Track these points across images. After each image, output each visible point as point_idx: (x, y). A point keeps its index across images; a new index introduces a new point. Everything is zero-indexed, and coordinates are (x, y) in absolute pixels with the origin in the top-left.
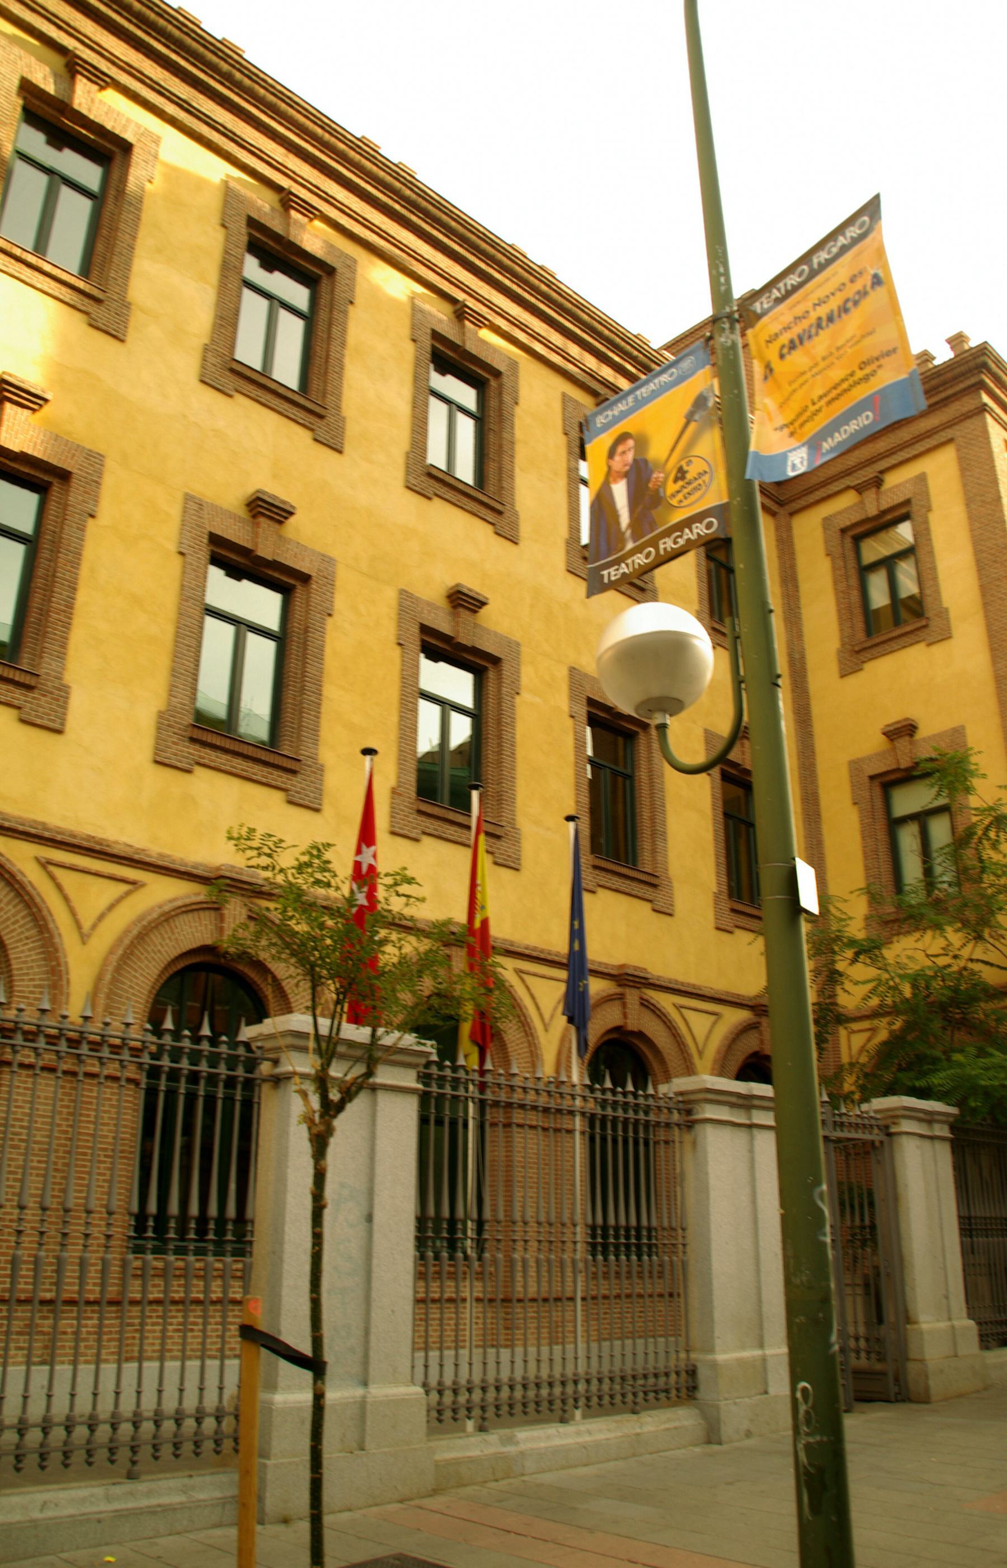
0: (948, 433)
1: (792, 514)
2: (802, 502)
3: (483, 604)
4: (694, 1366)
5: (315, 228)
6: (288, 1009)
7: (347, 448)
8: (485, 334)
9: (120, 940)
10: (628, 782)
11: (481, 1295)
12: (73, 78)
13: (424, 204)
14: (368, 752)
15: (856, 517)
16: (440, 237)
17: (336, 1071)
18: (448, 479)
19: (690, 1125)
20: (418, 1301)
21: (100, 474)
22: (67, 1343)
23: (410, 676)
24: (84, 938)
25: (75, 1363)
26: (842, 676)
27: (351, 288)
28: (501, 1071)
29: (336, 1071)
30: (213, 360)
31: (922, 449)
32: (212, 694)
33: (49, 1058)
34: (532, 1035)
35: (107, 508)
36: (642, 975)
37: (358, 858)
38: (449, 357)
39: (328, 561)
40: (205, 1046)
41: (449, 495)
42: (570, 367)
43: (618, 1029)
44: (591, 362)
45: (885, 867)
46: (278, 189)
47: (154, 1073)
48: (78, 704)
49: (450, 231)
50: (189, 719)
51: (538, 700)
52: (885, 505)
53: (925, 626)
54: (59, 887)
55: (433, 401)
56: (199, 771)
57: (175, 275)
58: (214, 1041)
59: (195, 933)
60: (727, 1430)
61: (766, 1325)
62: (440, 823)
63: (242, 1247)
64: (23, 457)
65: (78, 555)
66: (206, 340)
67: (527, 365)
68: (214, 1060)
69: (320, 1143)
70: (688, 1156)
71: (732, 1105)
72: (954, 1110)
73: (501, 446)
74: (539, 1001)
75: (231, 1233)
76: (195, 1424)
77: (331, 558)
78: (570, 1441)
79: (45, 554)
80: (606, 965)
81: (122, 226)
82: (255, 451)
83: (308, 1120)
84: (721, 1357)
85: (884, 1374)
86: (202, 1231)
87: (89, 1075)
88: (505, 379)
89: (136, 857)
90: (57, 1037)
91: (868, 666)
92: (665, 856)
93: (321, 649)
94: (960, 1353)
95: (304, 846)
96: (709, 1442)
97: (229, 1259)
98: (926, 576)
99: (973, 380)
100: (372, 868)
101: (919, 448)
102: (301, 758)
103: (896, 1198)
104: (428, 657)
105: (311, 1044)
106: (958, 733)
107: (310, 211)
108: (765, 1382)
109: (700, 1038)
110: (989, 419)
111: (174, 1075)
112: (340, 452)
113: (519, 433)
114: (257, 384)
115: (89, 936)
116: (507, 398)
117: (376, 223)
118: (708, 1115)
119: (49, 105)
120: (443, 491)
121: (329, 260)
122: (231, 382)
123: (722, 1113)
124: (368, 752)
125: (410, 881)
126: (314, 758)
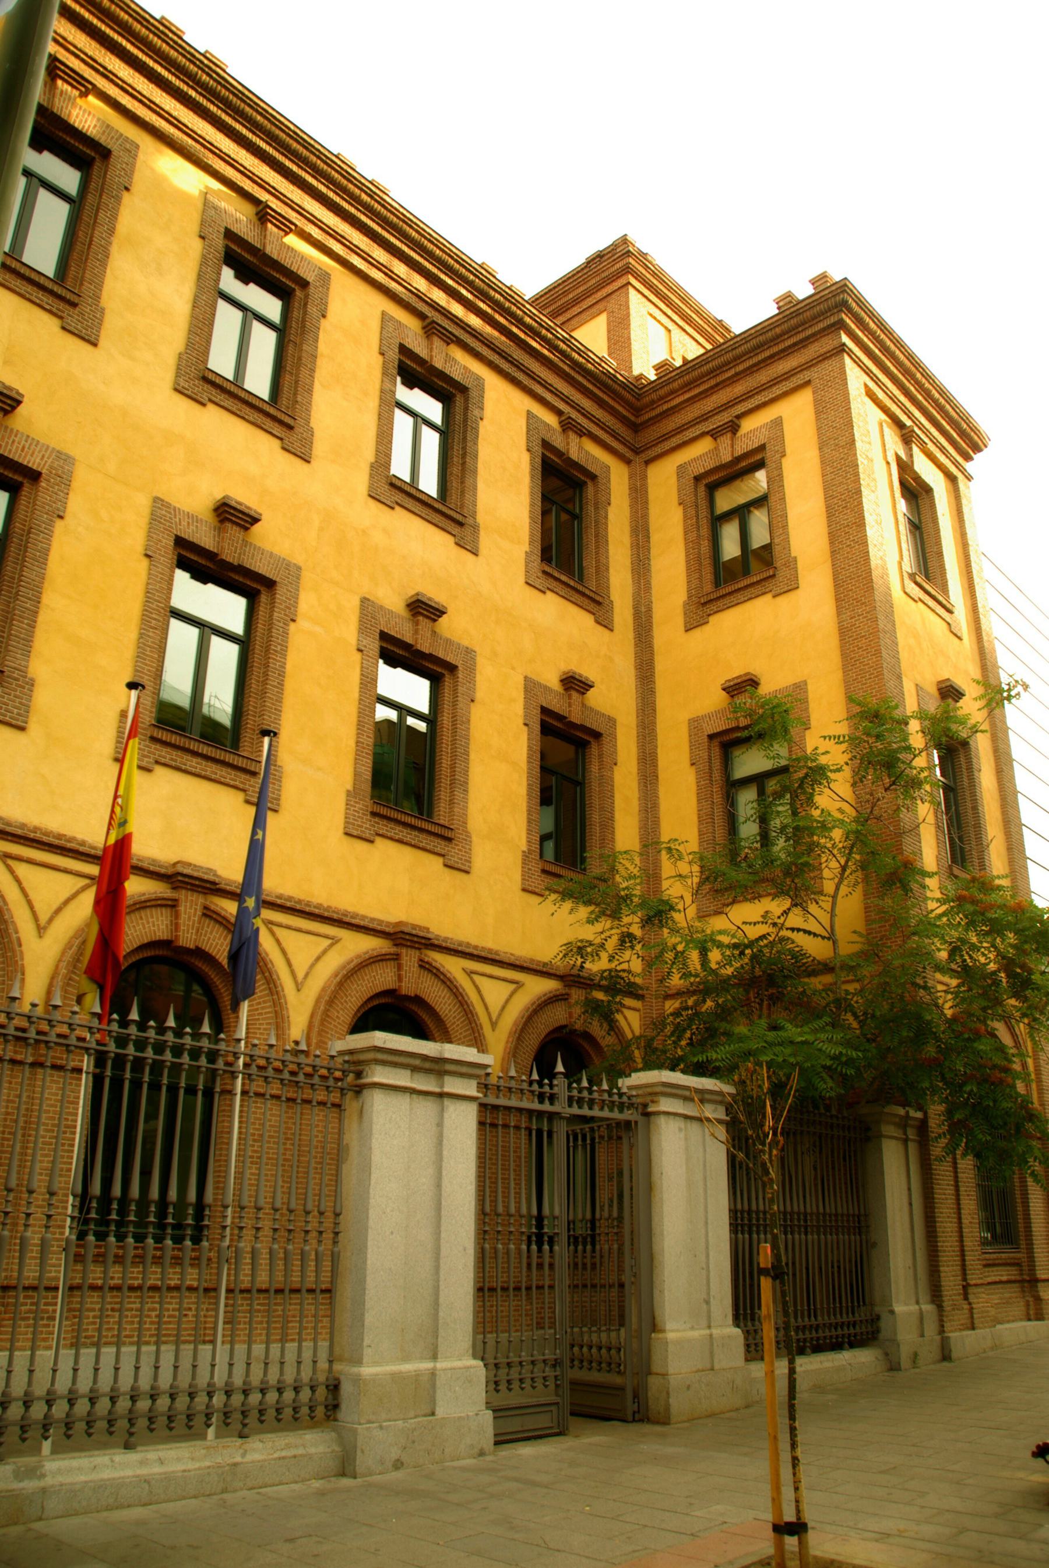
0: (806, 376)
1: (648, 462)
2: (658, 450)
3: (255, 520)
4: (338, 1380)
7: (103, 342)
8: (292, 240)
10: (578, 789)
11: (195, 1284)
13: (224, 92)
15: (710, 464)
16: (244, 131)
18: (413, 491)
19: (359, 1090)
23: (369, 681)
26: (687, 631)
27: (129, 171)
28: (524, 1078)
31: (779, 392)
34: (277, 993)
36: (421, 934)
40: (170, 1037)
41: (228, 403)
42: (393, 285)
43: (390, 993)
44: (420, 283)
45: (720, 833)
48: (43, 698)
51: (317, 629)
52: (739, 451)
53: (774, 576)
60: (364, 1461)
61: (442, 1333)
70: (355, 1125)
71: (415, 1069)
72: (728, 1089)
73: (300, 359)
74: (290, 956)
77: (69, 457)
78: (129, 1472)
80: (380, 922)
84: (367, 1371)
85: (622, 1389)
87: (257, 1094)
88: (312, 290)
91: (713, 619)
92: (465, 808)
93: (46, 552)
94: (717, 1366)
96: (343, 1474)
98: (778, 525)
99: (832, 320)
101: (777, 391)
103: (650, 1188)
104: (386, 663)
106: (800, 689)
107: (86, 88)
108: (433, 1401)
109: (495, 1011)
110: (847, 360)
111: (138, 1064)
112: (95, 345)
113: (322, 347)
114: (227, 394)
115: (45, 928)
116: (312, 310)
117: (167, 108)
118: (377, 1079)
120: (220, 397)
121: (103, 140)
122: (206, 392)
123: (402, 1078)
126: (23, 671)
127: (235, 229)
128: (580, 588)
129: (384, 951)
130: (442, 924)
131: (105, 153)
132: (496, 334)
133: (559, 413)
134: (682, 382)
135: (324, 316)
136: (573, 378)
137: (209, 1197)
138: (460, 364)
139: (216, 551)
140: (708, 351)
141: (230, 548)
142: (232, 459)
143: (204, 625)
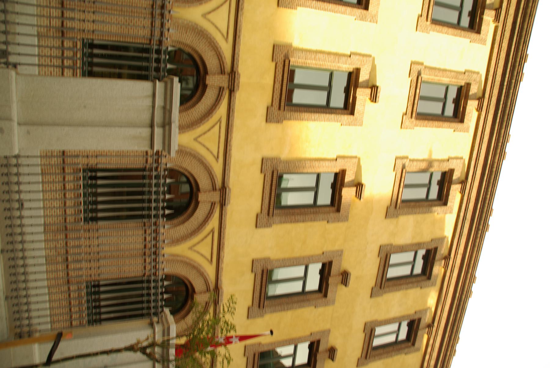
3: (333, 359)
5: (441, 270)
6: (177, 322)
7: (373, 300)
9: (192, 260)
14: (272, 332)
17: (157, 350)
18: (386, 267)
20: (64, 152)
21: (342, 221)
22: (53, 267)
23: (302, 340)
24: (191, 248)
27: (427, 286)
29: (157, 350)
30: (388, 248)
32: (280, 274)
33: (149, 245)
35: (332, 226)
37: (234, 337)
38: (414, 326)
39: (333, 302)
40: (162, 197)
46: (450, 254)
47: (149, 281)
48: (267, 231)
49: (456, 315)
50: (269, 268)
54: (206, 237)
55: (397, 325)
56: (253, 275)
57: (411, 229)
58: (164, 200)
59: (198, 285)
62: (270, 182)
63: (91, 322)
64: (340, 197)
65: (315, 220)
66: (394, 244)
68: (156, 301)
69: (131, 348)
71: (164, 108)
75: (96, 318)
76: (14, 164)
79: (312, 210)
81: (421, 209)
82: (363, 269)
83: (138, 342)
86: (91, 178)
87: (145, 260)
88: (412, 348)
89: (220, 260)
90: (156, 247)
93: (304, 307)
95: (233, 322)
97: (85, 298)
100: (231, 342)
104: (309, 345)
105: (166, 338)
107: (446, 266)
114: (385, 264)
116: (406, 350)
119: (450, 178)
120: (383, 262)
122: (383, 255)
124: (272, 332)
125: (229, 362)
130: (240, 96)
131: (429, 278)
137: (101, 223)
142: (364, 271)
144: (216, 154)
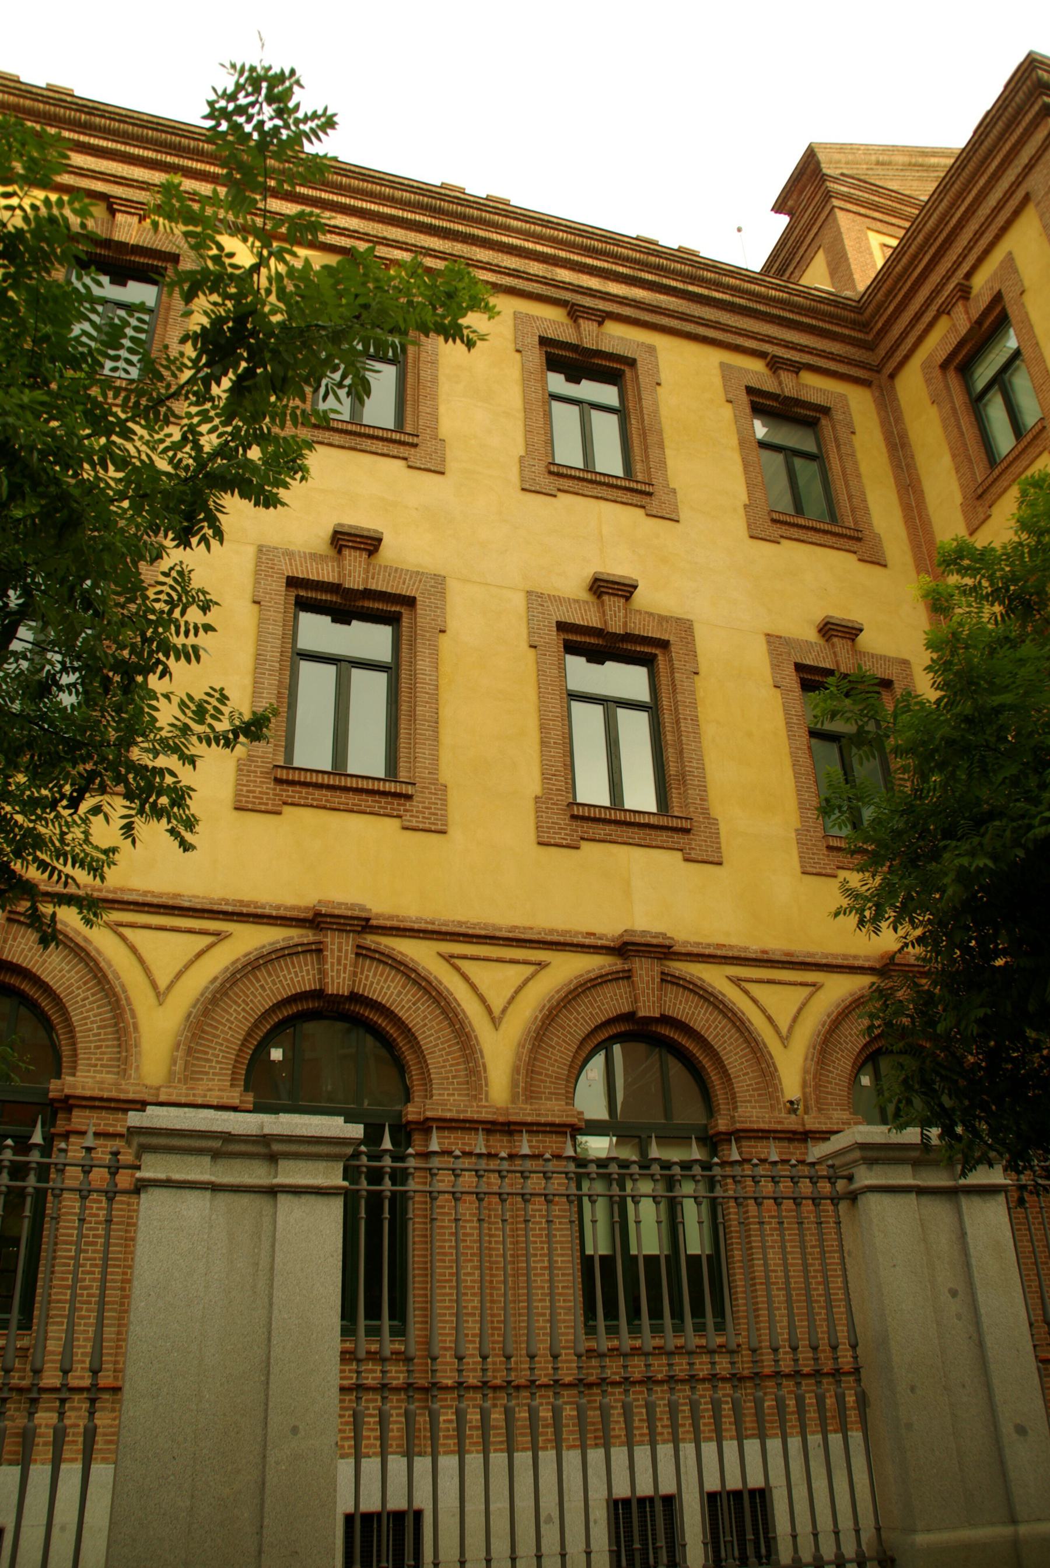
1: (892, 376)
7: (684, 514)
12: (114, 216)
25: (510, 1452)
39: (686, 627)
59: (298, 977)
67: (661, 342)
71: (216, 1155)
79: (667, 718)
82: (587, 542)
102: (692, 815)
115: (501, 1019)
122: (777, 531)
127: (550, 335)
128: (836, 530)
129: (607, 969)
130: (380, 901)
132: (898, 359)
133: (761, 355)
134: (900, 275)
135: (853, 433)
136: (756, 311)
138: (617, 337)
139: (606, 631)
140: (908, 230)
141: (354, 573)
143: (340, 661)
144: (529, 970)
